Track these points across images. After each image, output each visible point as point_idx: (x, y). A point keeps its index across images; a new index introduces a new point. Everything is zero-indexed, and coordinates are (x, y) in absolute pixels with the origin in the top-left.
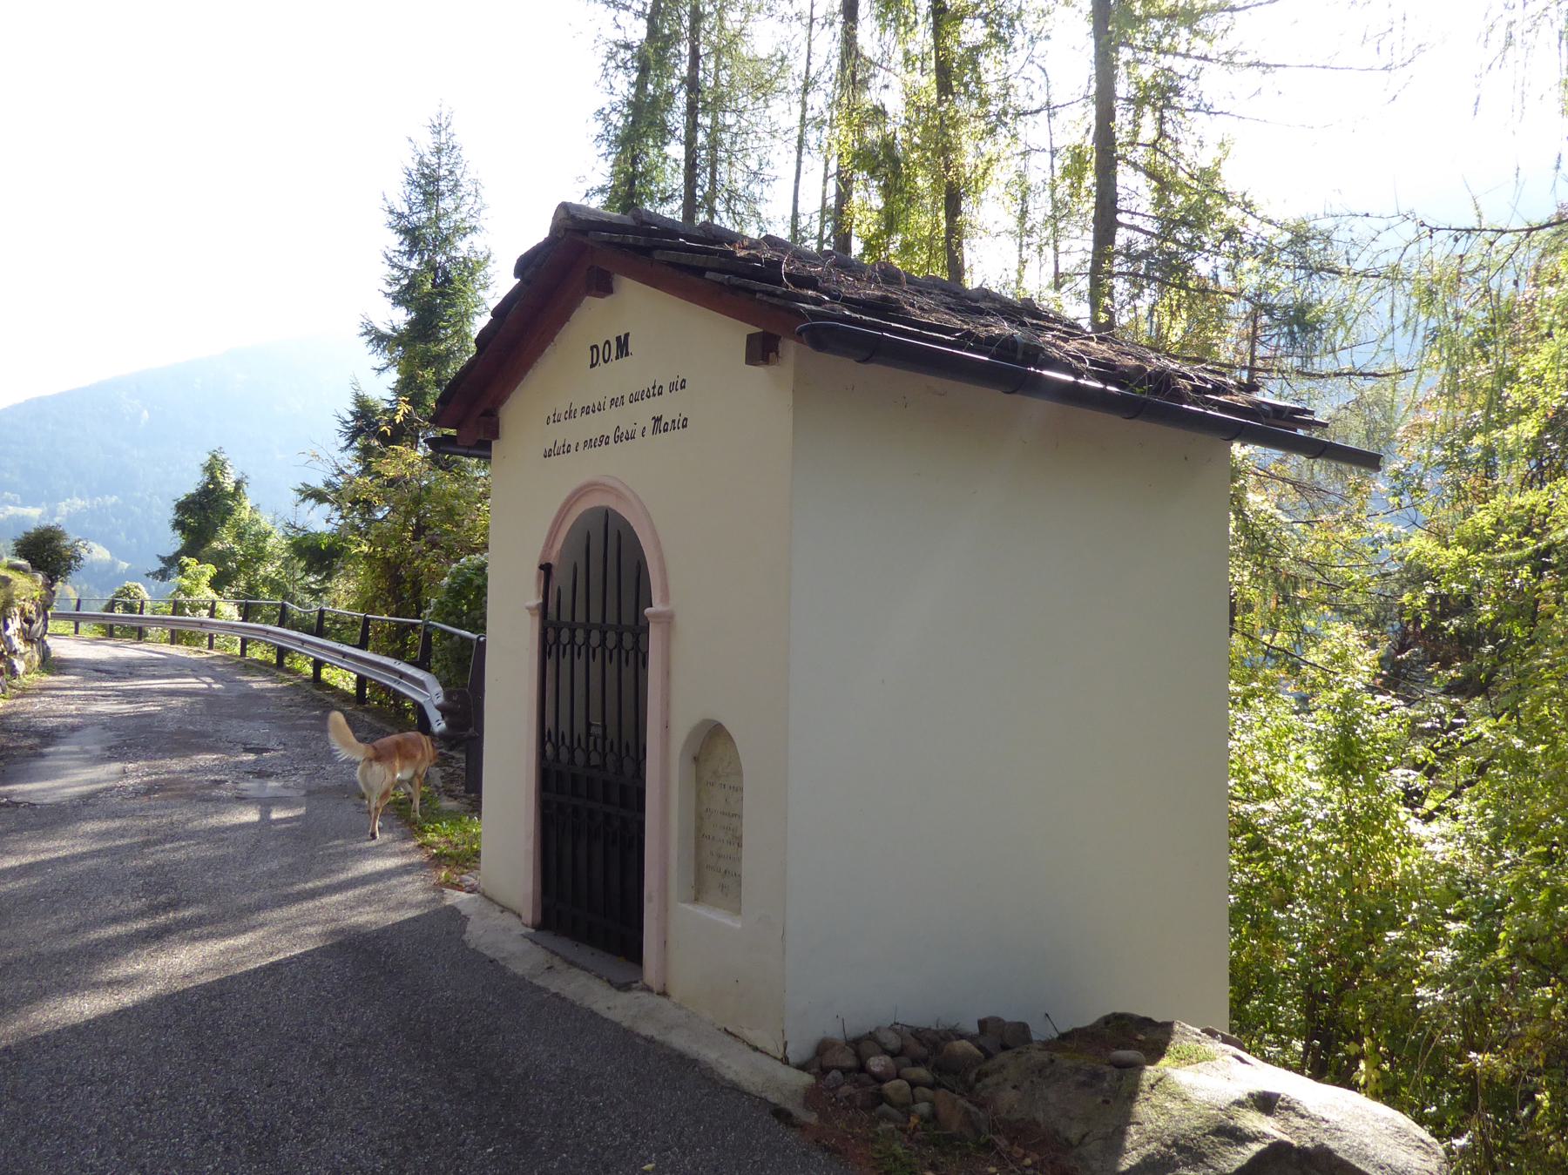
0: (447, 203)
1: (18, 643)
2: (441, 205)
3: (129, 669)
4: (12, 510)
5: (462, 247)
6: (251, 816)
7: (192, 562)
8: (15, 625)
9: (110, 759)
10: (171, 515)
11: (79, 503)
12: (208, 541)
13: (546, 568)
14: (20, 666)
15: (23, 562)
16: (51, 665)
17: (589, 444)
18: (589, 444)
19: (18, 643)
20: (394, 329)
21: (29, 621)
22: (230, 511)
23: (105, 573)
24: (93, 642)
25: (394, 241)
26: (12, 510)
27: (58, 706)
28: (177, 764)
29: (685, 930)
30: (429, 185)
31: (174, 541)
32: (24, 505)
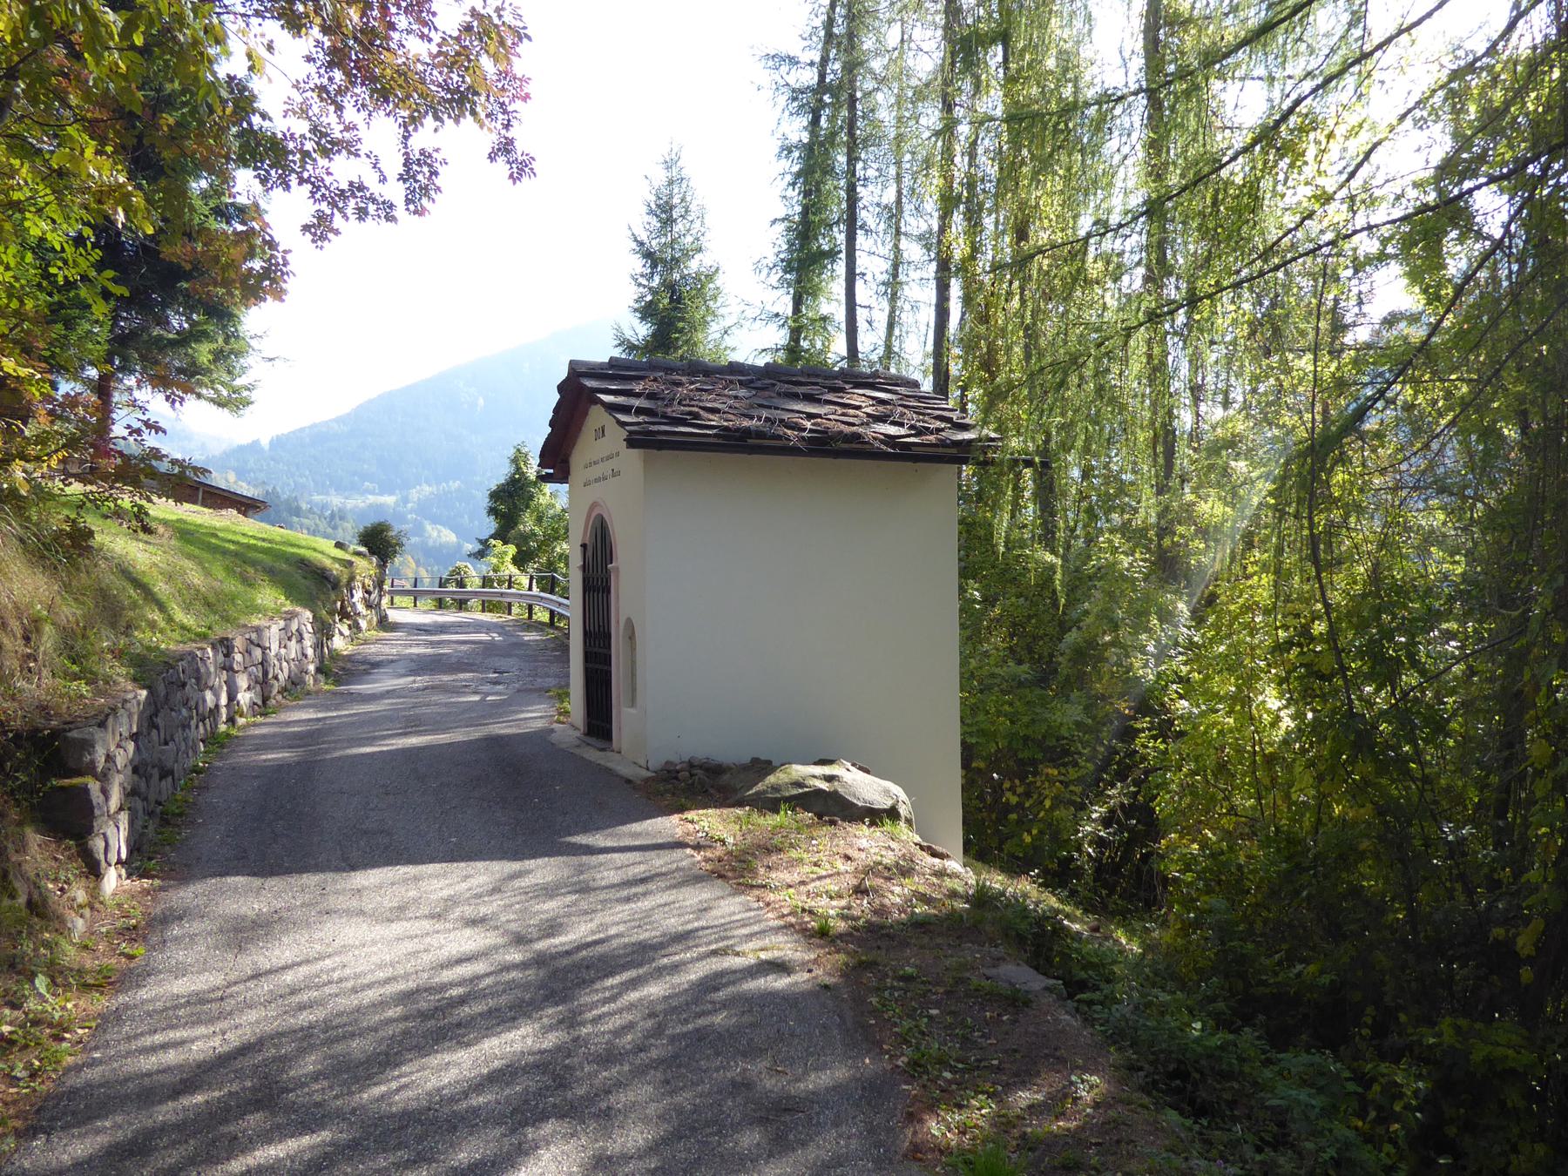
0: (679, 227)
1: (361, 607)
2: (676, 229)
3: (442, 628)
4: (371, 499)
5: (693, 266)
6: (477, 698)
7: (499, 543)
8: (358, 595)
9: (692, 931)
10: (485, 502)
11: (427, 489)
12: (516, 524)
13: (584, 546)
14: (363, 624)
15: (363, 549)
16: (384, 624)
17: (597, 480)
18: (597, 480)
19: (361, 607)
20: (631, 347)
21: (369, 592)
22: (531, 497)
23: (433, 553)
24: (426, 612)
25: (638, 265)
26: (371, 499)
27: (386, 650)
28: (446, 678)
29: (624, 717)
30: (665, 213)
31: (490, 525)
32: (381, 494)
